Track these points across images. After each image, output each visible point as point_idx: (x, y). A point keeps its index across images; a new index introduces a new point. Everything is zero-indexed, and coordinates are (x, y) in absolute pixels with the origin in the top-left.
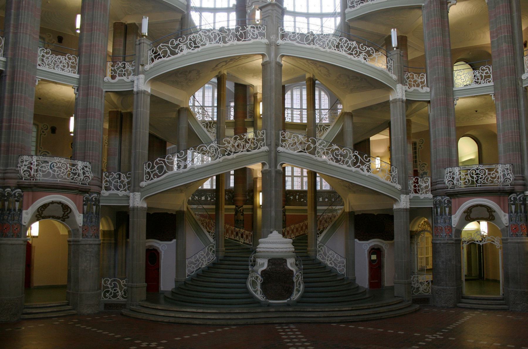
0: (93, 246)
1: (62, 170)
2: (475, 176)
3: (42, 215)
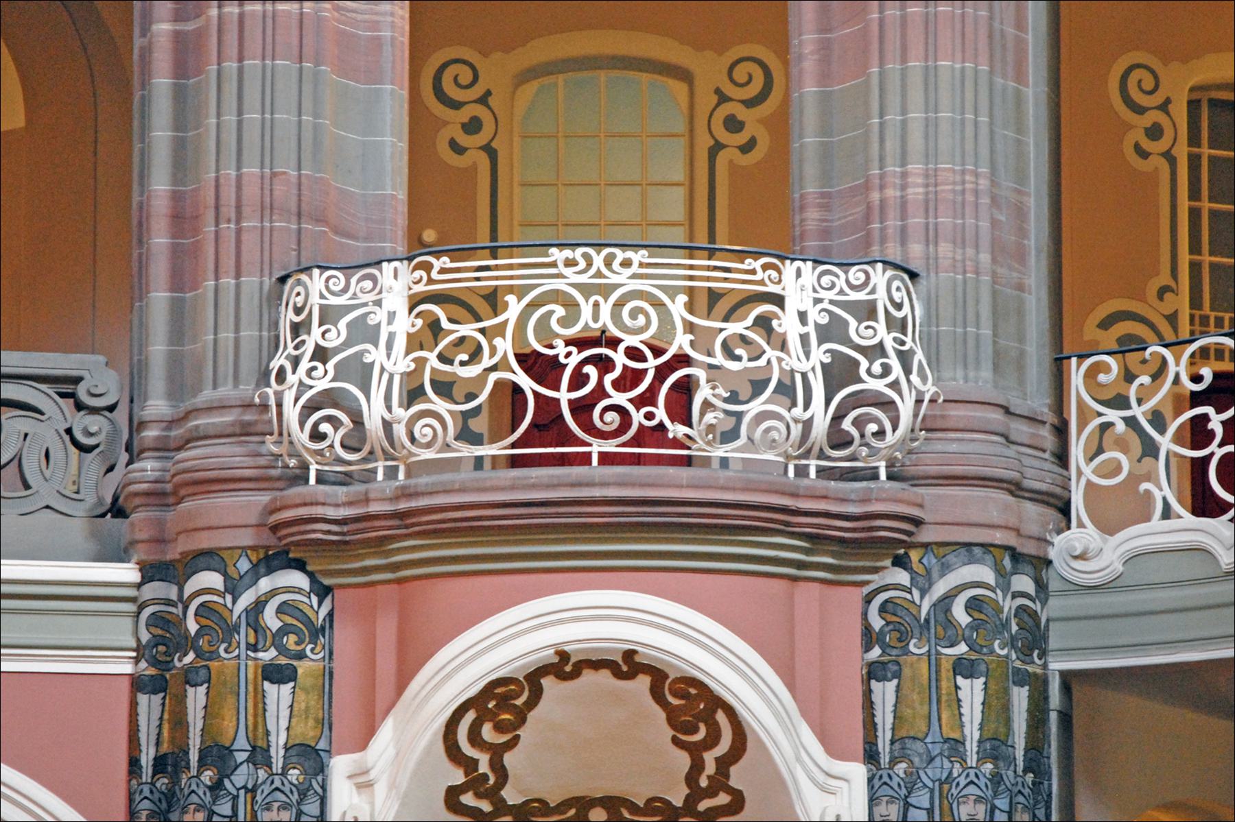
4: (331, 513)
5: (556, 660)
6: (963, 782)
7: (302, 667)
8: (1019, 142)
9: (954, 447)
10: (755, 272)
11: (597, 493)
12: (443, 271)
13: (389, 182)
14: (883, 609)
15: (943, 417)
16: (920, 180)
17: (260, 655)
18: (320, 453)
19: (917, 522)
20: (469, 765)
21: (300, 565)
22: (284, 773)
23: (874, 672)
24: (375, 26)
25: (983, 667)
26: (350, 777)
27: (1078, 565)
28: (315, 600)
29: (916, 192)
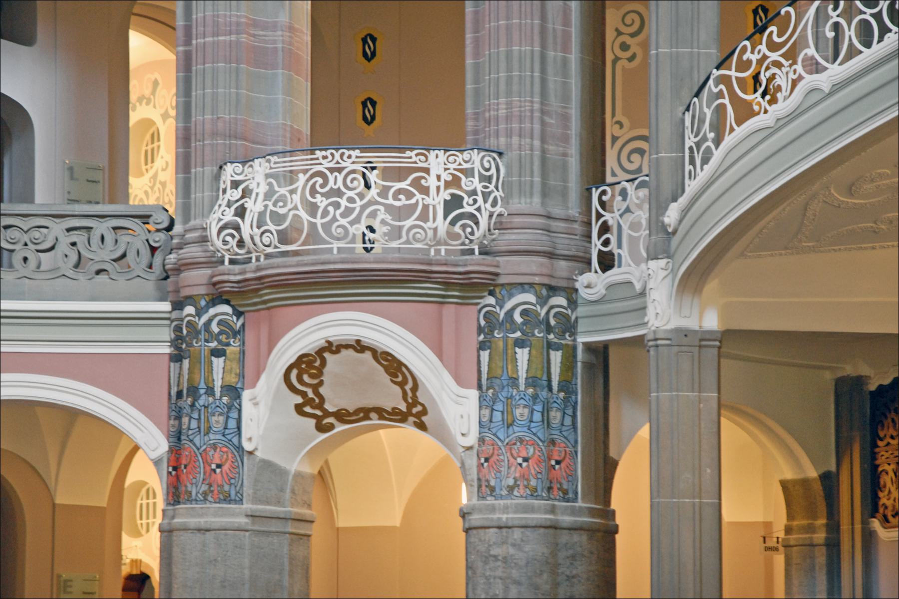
0: (517, 534)
1: (344, 202)
2: (322, 202)
3: (403, 407)
4: (232, 278)
5: (327, 345)
6: (518, 398)
7: (229, 350)
8: (565, 83)
9: (513, 237)
10: (412, 157)
11: (332, 267)
12: (275, 163)
13: (280, 116)
14: (485, 317)
15: (510, 222)
16: (504, 106)
17: (210, 344)
18: (229, 250)
19: (497, 275)
20: (304, 394)
21: (227, 302)
22: (220, 399)
23: (482, 346)
24: (275, 42)
25: (528, 343)
26: (251, 400)
27: (588, 291)
28: (235, 318)
29: (502, 112)
